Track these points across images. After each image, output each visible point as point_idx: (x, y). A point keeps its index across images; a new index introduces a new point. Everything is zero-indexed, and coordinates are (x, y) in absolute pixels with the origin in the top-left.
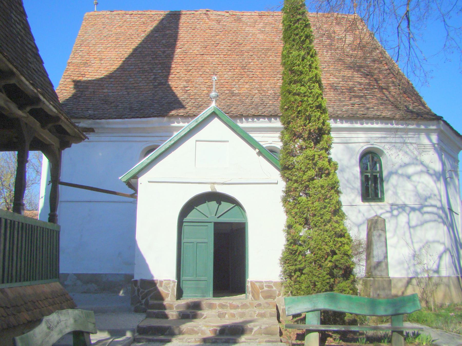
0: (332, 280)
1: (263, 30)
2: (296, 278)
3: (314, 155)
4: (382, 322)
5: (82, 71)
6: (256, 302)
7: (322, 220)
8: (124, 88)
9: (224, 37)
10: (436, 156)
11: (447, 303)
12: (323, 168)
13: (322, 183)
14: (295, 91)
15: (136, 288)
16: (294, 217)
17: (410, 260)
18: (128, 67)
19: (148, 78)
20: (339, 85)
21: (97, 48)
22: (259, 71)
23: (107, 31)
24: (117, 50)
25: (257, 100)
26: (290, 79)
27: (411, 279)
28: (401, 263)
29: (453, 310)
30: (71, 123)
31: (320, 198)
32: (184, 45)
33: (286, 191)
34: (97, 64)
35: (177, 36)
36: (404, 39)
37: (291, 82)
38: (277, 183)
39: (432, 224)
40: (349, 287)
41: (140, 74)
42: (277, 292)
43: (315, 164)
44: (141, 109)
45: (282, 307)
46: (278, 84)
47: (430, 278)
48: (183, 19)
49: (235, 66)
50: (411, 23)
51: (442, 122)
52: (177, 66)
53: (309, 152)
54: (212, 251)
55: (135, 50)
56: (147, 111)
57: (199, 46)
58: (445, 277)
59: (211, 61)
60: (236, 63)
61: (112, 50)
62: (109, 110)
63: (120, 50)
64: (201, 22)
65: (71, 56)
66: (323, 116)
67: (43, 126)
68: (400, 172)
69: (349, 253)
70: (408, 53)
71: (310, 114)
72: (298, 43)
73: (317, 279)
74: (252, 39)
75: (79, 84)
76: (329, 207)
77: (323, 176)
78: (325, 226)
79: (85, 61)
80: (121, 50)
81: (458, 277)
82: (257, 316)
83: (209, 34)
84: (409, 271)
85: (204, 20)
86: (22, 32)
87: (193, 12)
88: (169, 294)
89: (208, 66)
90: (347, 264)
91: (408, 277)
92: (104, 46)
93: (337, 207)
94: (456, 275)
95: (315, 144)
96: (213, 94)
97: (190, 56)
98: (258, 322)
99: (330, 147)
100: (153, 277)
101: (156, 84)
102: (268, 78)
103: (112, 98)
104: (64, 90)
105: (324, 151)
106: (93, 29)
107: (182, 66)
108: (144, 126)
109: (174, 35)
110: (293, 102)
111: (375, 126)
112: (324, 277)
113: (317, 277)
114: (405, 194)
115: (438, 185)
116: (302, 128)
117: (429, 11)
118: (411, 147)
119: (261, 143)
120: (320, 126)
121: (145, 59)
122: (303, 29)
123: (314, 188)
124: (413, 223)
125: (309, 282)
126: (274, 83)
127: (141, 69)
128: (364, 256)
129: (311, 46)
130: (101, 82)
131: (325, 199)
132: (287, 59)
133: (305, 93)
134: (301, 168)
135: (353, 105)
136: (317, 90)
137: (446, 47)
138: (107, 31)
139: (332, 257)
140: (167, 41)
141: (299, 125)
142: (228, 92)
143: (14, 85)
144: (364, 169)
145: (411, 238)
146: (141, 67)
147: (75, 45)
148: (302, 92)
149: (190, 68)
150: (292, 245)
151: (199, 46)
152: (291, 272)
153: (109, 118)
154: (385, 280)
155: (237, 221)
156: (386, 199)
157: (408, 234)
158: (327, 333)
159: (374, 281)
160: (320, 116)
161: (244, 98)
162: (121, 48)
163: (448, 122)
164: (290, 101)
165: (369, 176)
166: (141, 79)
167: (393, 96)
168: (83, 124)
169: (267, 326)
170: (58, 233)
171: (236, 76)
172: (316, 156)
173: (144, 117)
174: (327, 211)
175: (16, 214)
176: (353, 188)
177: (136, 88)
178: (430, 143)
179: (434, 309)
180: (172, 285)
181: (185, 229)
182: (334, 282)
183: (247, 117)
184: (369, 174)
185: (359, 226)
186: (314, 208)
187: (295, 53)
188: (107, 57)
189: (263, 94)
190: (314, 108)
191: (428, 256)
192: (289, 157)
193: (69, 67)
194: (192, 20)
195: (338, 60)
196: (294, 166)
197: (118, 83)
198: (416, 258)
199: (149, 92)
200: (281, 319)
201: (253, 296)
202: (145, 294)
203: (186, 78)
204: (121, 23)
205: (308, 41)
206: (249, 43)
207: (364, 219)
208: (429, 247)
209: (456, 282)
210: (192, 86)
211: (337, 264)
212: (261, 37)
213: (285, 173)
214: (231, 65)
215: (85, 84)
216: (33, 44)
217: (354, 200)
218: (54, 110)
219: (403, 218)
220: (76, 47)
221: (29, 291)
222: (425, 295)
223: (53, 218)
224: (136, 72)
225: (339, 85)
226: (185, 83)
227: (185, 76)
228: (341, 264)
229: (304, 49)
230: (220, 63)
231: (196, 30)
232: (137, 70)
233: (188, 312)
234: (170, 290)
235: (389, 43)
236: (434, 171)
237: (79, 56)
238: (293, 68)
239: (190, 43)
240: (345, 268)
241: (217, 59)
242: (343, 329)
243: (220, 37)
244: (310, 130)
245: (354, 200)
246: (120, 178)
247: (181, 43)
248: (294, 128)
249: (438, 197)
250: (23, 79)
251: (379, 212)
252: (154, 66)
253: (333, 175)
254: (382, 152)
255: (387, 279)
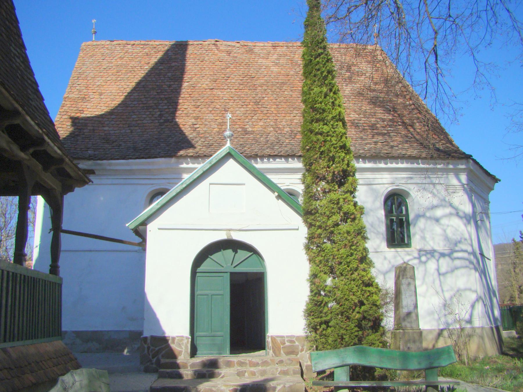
0: (360, 333)
1: (278, 62)
2: (322, 331)
3: (339, 199)
4: (414, 377)
5: (80, 106)
6: (277, 359)
7: (349, 269)
8: (127, 126)
9: (235, 70)
10: (465, 197)
11: (481, 356)
12: (348, 213)
13: (348, 229)
14: (317, 130)
15: (146, 346)
16: (318, 266)
17: (440, 310)
18: (130, 103)
19: (153, 115)
20: (361, 122)
21: (96, 81)
22: (274, 107)
23: (106, 63)
24: (118, 84)
25: (273, 138)
26: (311, 117)
27: (442, 330)
28: (431, 313)
29: (488, 363)
30: (74, 164)
31: (346, 245)
32: (191, 78)
33: (310, 238)
34: (97, 100)
35: (184, 68)
36: (432, 74)
37: (312, 121)
38: (298, 229)
39: (463, 271)
40: (378, 340)
41: (144, 110)
42: (300, 348)
43: (340, 209)
44: (147, 149)
45: (305, 364)
46: (295, 121)
47: (462, 329)
48: (190, 50)
49: (248, 101)
50: (438, 58)
51: (471, 161)
52: (184, 101)
53: (333, 196)
54: (228, 304)
55: (138, 84)
56: (153, 151)
57: (208, 80)
58: (479, 327)
59: (222, 96)
60: (249, 99)
61: (113, 84)
62: (111, 150)
63: (122, 84)
64: (210, 54)
65: (67, 91)
66: (348, 157)
67: (46, 168)
68: (428, 214)
69: (378, 303)
70: (436, 89)
71: (333, 155)
72: (320, 78)
73: (344, 332)
74: (266, 72)
75: (77, 121)
76: (356, 254)
77: (349, 220)
78: (351, 274)
79: (83, 96)
80: (123, 84)
81: (492, 328)
82: (279, 373)
83: (219, 67)
84: (440, 322)
85: (213, 52)
86: (21, 66)
87: (200, 42)
88: (182, 351)
89: (218, 101)
90: (376, 315)
91: (439, 329)
92: (104, 79)
93: (364, 254)
94: (490, 326)
95: (339, 187)
96: (228, 133)
97: (198, 91)
98: (280, 380)
99: (355, 189)
100: (164, 333)
101: (162, 121)
102: (283, 115)
103: (114, 137)
104: (63, 128)
105: (349, 194)
106: (91, 60)
107: (190, 101)
108: (150, 167)
109: (180, 67)
110: (315, 142)
111: (400, 165)
112: (352, 329)
113: (345, 329)
114: (433, 239)
115: (469, 228)
116: (325, 169)
117: (457, 44)
118: (438, 187)
119: (279, 185)
120: (345, 167)
121: (149, 94)
122: (325, 64)
123: (340, 233)
124: (443, 270)
125: (337, 336)
126: (293, 119)
127: (145, 105)
128: (392, 307)
129: (333, 82)
130: (101, 119)
131: (352, 246)
132: (308, 96)
133: (328, 132)
134: (325, 213)
135: (376, 143)
136: (341, 130)
137: (476, 83)
138: (106, 63)
139: (360, 307)
140: (173, 74)
141: (322, 166)
142: (240, 130)
143: (18, 125)
144: (389, 212)
145: (441, 286)
146: (145, 102)
147: (71, 78)
148: (325, 131)
149: (199, 104)
150: (317, 295)
151: (208, 80)
152: (317, 325)
153: (112, 159)
154: (415, 332)
155: (255, 271)
156: (413, 244)
157: (437, 282)
158: (355, 390)
159: (404, 334)
160: (344, 157)
161: (258, 136)
162: (122, 81)
163: (478, 161)
164: (312, 141)
165: (395, 220)
166: (144, 116)
167: (418, 133)
168: (84, 165)
169: (291, 384)
170: (60, 285)
171: (249, 112)
172: (341, 200)
173: (149, 158)
174: (354, 259)
175: (18, 266)
176: (378, 233)
177: (140, 125)
178: (459, 184)
179: (468, 363)
180: (185, 341)
181: (199, 279)
182: (363, 334)
183: (262, 157)
184: (394, 218)
185: (385, 274)
186: (340, 256)
187: (317, 90)
188: (108, 92)
189: (279, 132)
190: (338, 148)
191: (460, 305)
192: (312, 201)
193: (66, 103)
194: (200, 52)
195: (359, 95)
196: (318, 211)
197: (120, 120)
198: (447, 308)
199: (155, 130)
200: (305, 376)
201: (274, 352)
202: (156, 353)
203: (194, 115)
204: (122, 54)
205: (330, 77)
206: (262, 76)
207: (390, 266)
208: (460, 295)
209: (490, 332)
210: (202, 123)
211: (365, 315)
212: (275, 69)
213: (308, 218)
214: (243, 101)
215: (83, 121)
216: (32, 79)
217: (379, 246)
218: (59, 151)
219: (432, 265)
220: (73, 81)
221: (32, 350)
222: (457, 348)
223: (54, 269)
224: (140, 108)
225: (361, 122)
226: (193, 120)
227: (193, 112)
228: (370, 315)
229: (327, 85)
230: (231, 99)
231: (204, 62)
232: (141, 105)
233: (205, 370)
234: (183, 347)
235: (416, 78)
236: (464, 213)
237: (76, 90)
238: (315, 106)
239: (198, 76)
240: (374, 319)
241: (228, 94)
242: (375, 385)
243: (231, 70)
244: (334, 172)
245: (379, 246)
246: (127, 225)
247: (189, 76)
248: (317, 170)
249: (469, 242)
250: (28, 118)
251: (407, 258)
252: (160, 102)
253: (359, 220)
254: (408, 194)
255: (417, 331)
